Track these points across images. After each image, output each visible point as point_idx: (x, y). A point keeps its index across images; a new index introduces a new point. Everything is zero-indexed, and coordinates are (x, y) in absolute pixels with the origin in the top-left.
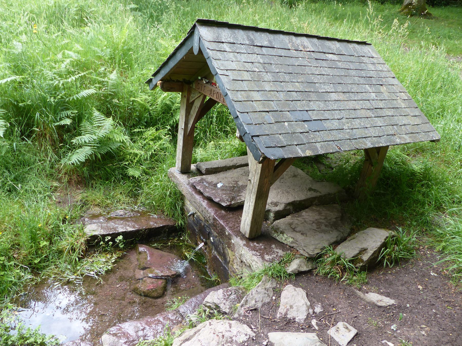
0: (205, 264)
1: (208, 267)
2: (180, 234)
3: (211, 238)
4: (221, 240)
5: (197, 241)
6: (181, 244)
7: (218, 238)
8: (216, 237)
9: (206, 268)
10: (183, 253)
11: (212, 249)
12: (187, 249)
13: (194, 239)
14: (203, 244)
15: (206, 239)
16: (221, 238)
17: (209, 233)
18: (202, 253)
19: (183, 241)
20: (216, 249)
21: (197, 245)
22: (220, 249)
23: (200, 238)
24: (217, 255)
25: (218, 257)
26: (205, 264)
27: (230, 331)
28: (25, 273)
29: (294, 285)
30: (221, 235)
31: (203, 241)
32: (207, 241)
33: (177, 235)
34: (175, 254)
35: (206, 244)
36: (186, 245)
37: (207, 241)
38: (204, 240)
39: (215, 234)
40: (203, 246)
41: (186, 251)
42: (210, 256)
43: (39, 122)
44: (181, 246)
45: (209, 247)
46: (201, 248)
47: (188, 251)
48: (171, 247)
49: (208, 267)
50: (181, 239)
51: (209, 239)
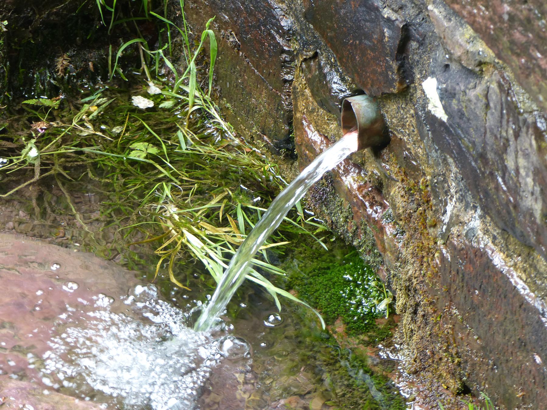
0: (376, 329)
1: (405, 357)
2: (131, 60)
3: (430, 87)
4: (521, 98)
5: (289, 120)
6: (140, 151)
7: (490, 81)
8: (475, 70)
9: (391, 364)
10: (162, 235)
11: (438, 190)
12: (203, 194)
13: (260, 100)
14: (350, 142)
15: (379, 99)
16: (525, 73)
17: (406, 34)
18: (347, 229)
19: (161, 124)
20: (482, 183)
21: (291, 151)
22: (515, 190)
23: (319, 85)
24: (484, 242)
25: (498, 260)
26: (376, 329)
27: (302, 396)
28: (494, 61)
29: (491, 260)
30: (522, 50)
31: (348, 121)
32: (392, 112)
33: (102, 70)
34: (87, 247)
35: (377, 140)
36: (193, 163)
37: (392, 112)
38: (361, 105)
39: (464, 40)
40: (354, 162)
41: (190, 220)
42: (423, 254)
43: (475, 408)
44: (145, 168)
45: (410, 169)
46: (332, 178)
47: (210, 215)
48: (46, 183)
49: (405, 357)
50: (141, 102)
51: (406, 91)
